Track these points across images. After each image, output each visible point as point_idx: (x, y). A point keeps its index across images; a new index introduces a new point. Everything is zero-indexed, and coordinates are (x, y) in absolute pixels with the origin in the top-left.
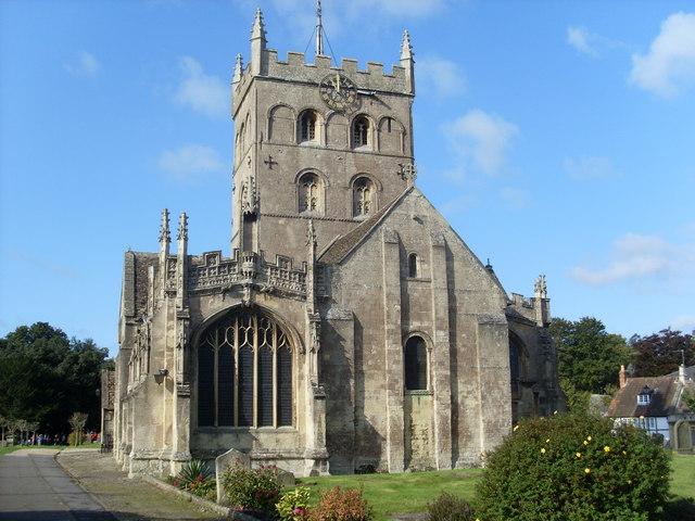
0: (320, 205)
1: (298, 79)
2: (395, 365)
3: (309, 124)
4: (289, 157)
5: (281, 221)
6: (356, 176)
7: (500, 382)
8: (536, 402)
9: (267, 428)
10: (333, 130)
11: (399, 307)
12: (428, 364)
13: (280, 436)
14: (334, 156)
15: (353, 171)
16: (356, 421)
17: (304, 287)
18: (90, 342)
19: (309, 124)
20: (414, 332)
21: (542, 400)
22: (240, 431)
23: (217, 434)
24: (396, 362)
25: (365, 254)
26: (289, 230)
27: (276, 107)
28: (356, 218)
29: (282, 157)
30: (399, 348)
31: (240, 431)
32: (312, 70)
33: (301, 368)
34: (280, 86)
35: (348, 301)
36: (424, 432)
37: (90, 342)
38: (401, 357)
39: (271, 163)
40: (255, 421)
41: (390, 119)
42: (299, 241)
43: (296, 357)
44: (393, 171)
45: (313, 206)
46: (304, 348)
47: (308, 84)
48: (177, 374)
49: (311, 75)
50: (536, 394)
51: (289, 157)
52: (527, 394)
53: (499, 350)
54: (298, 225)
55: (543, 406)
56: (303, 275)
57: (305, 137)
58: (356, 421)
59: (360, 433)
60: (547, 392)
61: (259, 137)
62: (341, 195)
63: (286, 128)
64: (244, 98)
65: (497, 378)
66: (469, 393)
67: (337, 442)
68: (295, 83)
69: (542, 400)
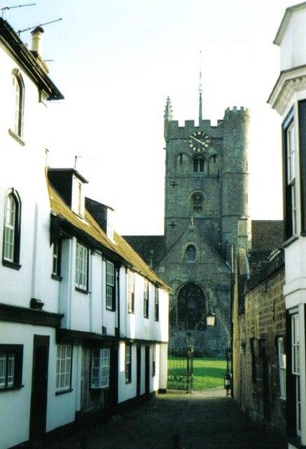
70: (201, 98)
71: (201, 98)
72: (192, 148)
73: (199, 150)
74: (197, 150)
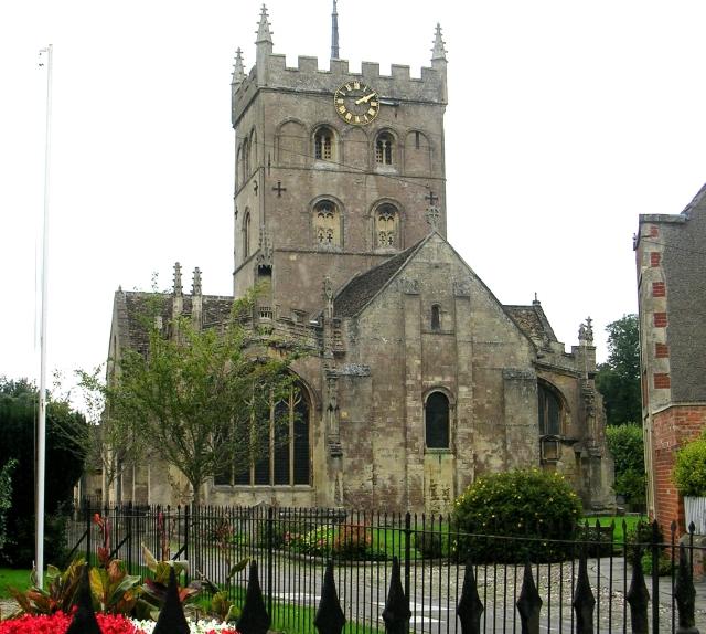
0: (336, 235)
1: (310, 88)
2: (418, 424)
3: (323, 142)
4: (301, 183)
5: (293, 257)
6: (378, 201)
7: (528, 441)
8: (577, 464)
9: (284, 486)
10: (352, 149)
11: (419, 362)
12: (451, 421)
13: (297, 495)
14: (353, 179)
15: (374, 196)
16: (374, 479)
17: (321, 343)
18: (23, 382)
19: (323, 142)
20: (436, 387)
21: (585, 461)
22: (257, 490)
23: (233, 493)
24: (416, 419)
25: (384, 306)
26: (302, 268)
28: (377, 251)
29: (292, 181)
30: (420, 405)
31: (257, 490)
32: (327, 78)
33: (318, 425)
34: (291, 99)
35: (366, 356)
36: (446, 493)
37: (23, 382)
38: (422, 414)
39: (280, 190)
40: (253, 479)
41: (417, 133)
42: (313, 279)
43: (313, 413)
44: (421, 195)
45: (330, 238)
46: (321, 405)
47: (321, 94)
48: (651, 382)
49: (325, 84)
50: (578, 454)
51: (301, 183)
52: (567, 453)
53: (528, 406)
54: (311, 262)
55: (585, 467)
56: (319, 330)
57: (319, 157)
58: (374, 479)
59: (378, 492)
60: (589, 452)
61: (267, 159)
62: (361, 225)
63: (297, 147)
64: (247, 109)
65: (525, 436)
66: (493, 451)
67: (355, 501)
68: (307, 94)
69: (585, 461)
70: (335, 16)
71: (335, 16)
72: (345, 114)
73: (358, 120)
74: (353, 119)
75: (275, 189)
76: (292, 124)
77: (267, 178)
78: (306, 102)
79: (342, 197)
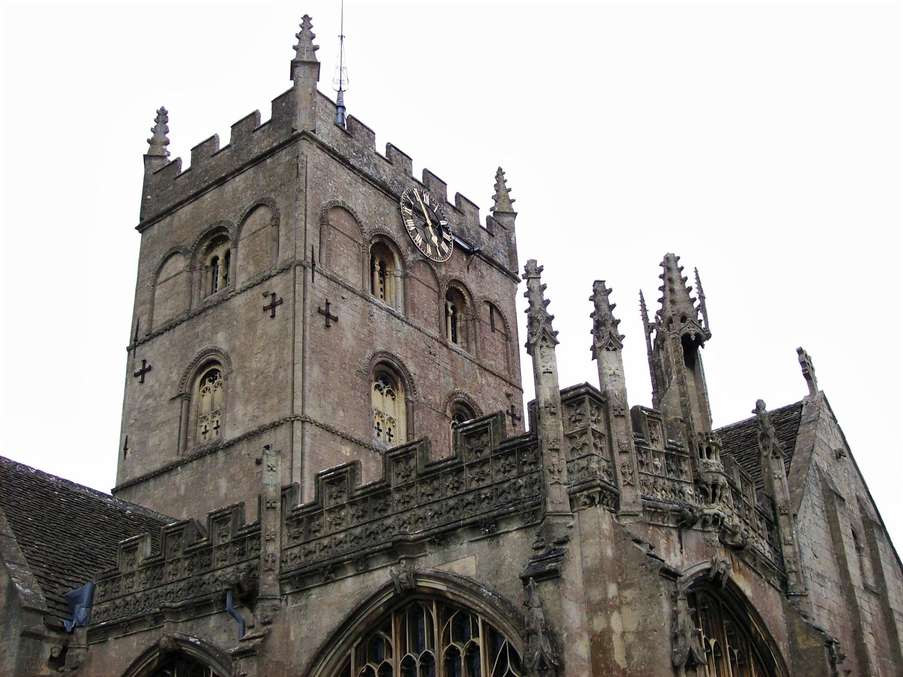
27: (336, 207)
61: (309, 254)
75: (320, 311)
76: (342, 213)
77: (309, 288)
78: (363, 189)
79: (411, 368)
